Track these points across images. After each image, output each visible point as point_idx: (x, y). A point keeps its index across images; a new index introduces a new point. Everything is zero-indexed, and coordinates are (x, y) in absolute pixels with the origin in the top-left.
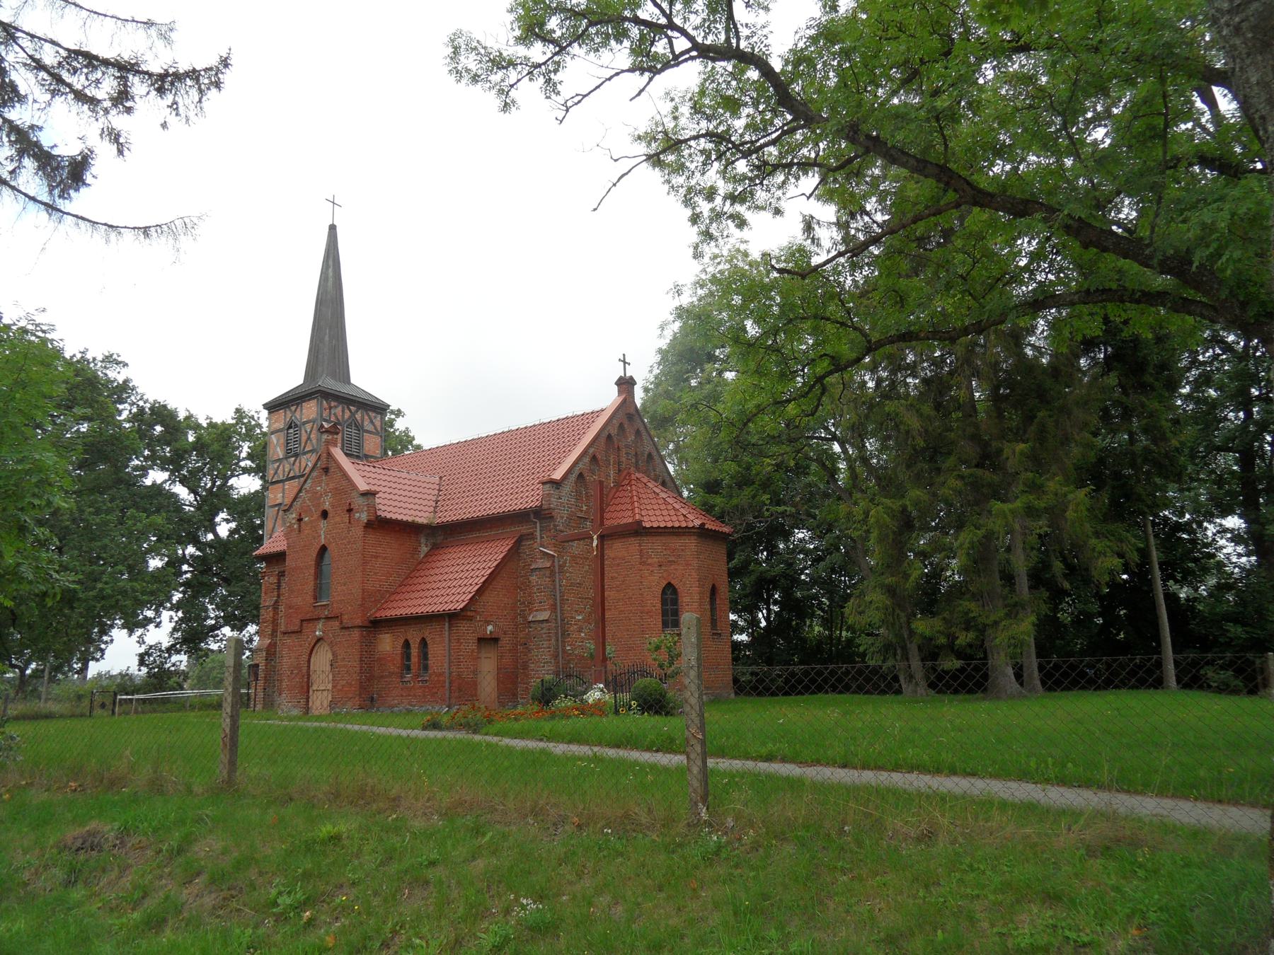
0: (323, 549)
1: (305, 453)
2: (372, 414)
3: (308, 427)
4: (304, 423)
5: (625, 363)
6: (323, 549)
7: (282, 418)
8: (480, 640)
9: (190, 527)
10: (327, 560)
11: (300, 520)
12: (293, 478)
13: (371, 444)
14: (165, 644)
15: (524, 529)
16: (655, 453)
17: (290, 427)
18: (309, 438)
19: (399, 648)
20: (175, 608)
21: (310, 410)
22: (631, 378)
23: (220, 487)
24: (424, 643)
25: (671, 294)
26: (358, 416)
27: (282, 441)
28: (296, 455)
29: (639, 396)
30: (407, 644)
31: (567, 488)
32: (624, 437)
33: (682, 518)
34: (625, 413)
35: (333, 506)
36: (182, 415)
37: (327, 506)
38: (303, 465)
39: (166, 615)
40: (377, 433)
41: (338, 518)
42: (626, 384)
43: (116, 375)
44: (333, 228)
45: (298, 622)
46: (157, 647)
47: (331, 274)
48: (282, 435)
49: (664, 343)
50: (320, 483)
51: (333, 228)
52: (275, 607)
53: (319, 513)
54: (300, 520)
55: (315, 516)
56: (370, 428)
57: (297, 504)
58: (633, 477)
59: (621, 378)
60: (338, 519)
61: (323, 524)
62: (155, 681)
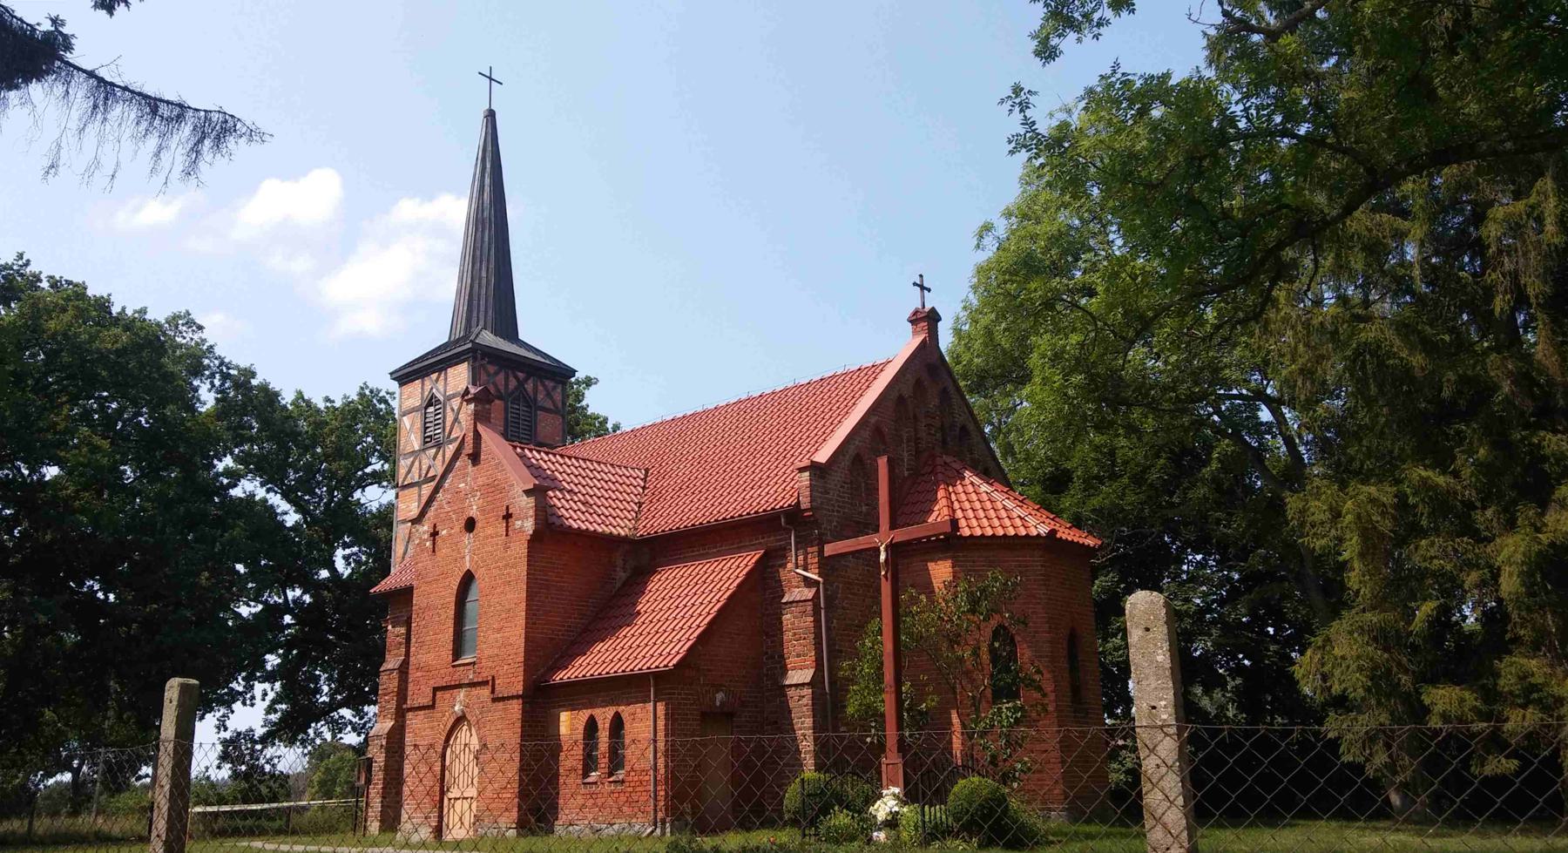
0: (468, 579)
2: (550, 384)
4: (449, 398)
5: (922, 288)
6: (468, 579)
7: (414, 394)
8: (703, 714)
9: (288, 557)
10: (474, 594)
11: (434, 534)
13: (547, 425)
14: (260, 731)
15: (772, 541)
16: (971, 427)
17: (430, 404)
18: (456, 420)
19: (581, 729)
20: (270, 677)
21: (459, 377)
22: (933, 310)
23: (339, 504)
25: (1007, 105)
26: (529, 386)
27: (419, 425)
29: (946, 340)
31: (836, 478)
32: (927, 415)
33: (1018, 522)
34: (926, 360)
36: (287, 398)
39: (259, 688)
40: (556, 411)
41: (490, 529)
42: (927, 319)
43: (186, 338)
44: (491, 115)
45: (429, 691)
46: (248, 735)
48: (418, 416)
49: (983, 256)
51: (491, 115)
52: (404, 669)
53: (463, 522)
54: (434, 534)
55: (457, 529)
56: (549, 405)
57: (431, 513)
58: (939, 461)
59: (916, 312)
60: (490, 531)
61: (467, 539)
62: (244, 785)
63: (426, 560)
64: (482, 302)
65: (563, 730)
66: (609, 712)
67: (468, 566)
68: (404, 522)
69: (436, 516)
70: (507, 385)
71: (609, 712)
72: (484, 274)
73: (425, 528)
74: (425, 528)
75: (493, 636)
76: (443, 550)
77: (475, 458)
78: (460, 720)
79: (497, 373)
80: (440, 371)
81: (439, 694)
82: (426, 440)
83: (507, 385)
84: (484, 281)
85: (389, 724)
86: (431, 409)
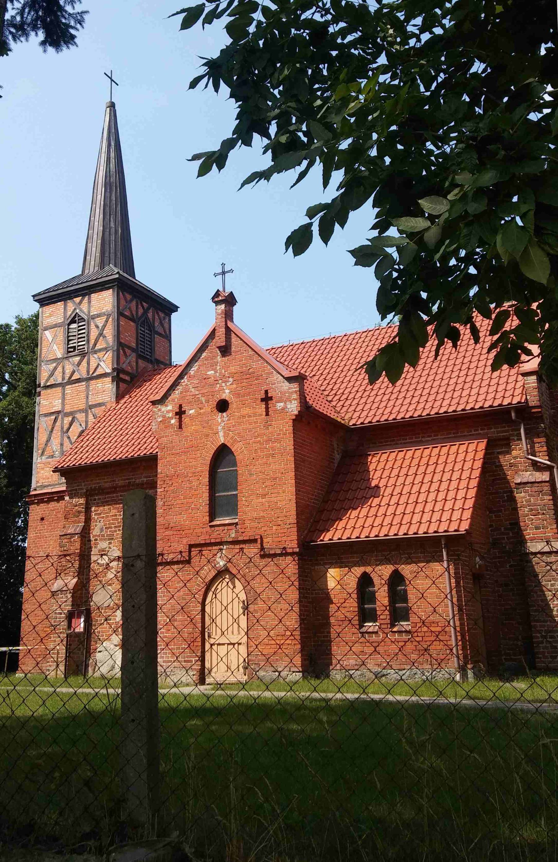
1: (96, 352)
3: (100, 322)
7: (55, 314)
11: (180, 413)
12: (78, 381)
17: (73, 321)
18: (101, 334)
24: (396, 579)
26: (150, 315)
28: (83, 355)
30: (365, 581)
35: (237, 395)
37: (226, 395)
38: (93, 365)
41: (247, 410)
44: (112, 106)
47: (112, 155)
50: (213, 366)
54: (180, 413)
57: (176, 394)
60: (246, 411)
61: (220, 417)
63: (170, 436)
64: (113, 246)
65: (331, 584)
66: (386, 570)
67: (222, 440)
68: (46, 415)
69: (182, 398)
70: (137, 312)
71: (386, 570)
72: (112, 225)
73: (169, 408)
74: (169, 408)
75: (256, 501)
76: (190, 427)
77: (225, 350)
78: (220, 574)
79: (131, 301)
80: (84, 296)
81: (195, 551)
82: (70, 350)
83: (137, 312)
84: (113, 230)
85: (72, 582)
86: (74, 326)
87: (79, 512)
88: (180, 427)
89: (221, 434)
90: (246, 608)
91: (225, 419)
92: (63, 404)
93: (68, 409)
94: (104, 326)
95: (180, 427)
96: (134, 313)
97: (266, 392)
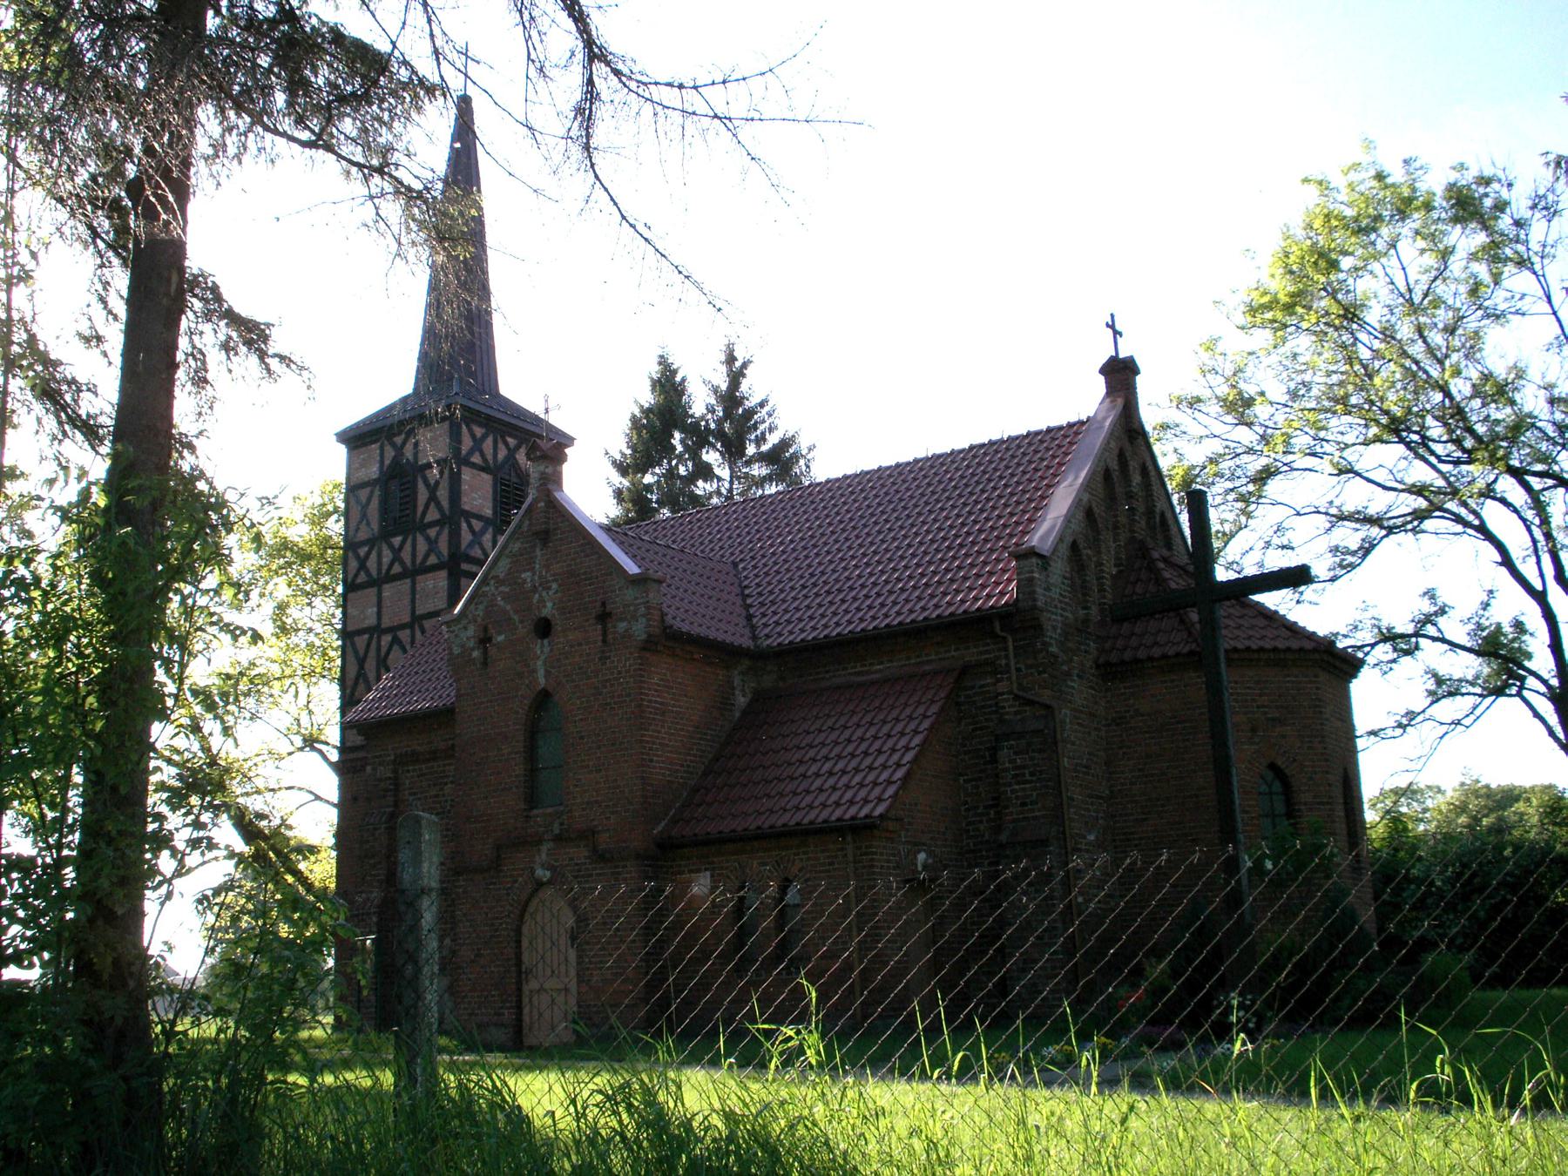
17: (392, 477)
37: (548, 610)
85: (376, 895)
87: (386, 790)
88: (485, 664)
89: (541, 673)
90: (573, 938)
91: (546, 650)
92: (379, 614)
93: (386, 623)
94: (369, 499)
95: (485, 664)
96: (490, 457)
97: (604, 604)
